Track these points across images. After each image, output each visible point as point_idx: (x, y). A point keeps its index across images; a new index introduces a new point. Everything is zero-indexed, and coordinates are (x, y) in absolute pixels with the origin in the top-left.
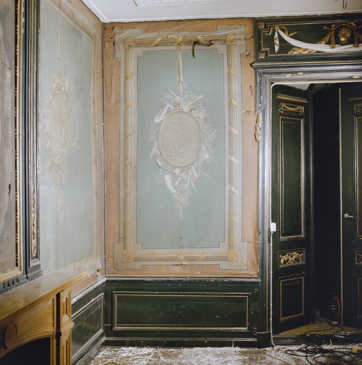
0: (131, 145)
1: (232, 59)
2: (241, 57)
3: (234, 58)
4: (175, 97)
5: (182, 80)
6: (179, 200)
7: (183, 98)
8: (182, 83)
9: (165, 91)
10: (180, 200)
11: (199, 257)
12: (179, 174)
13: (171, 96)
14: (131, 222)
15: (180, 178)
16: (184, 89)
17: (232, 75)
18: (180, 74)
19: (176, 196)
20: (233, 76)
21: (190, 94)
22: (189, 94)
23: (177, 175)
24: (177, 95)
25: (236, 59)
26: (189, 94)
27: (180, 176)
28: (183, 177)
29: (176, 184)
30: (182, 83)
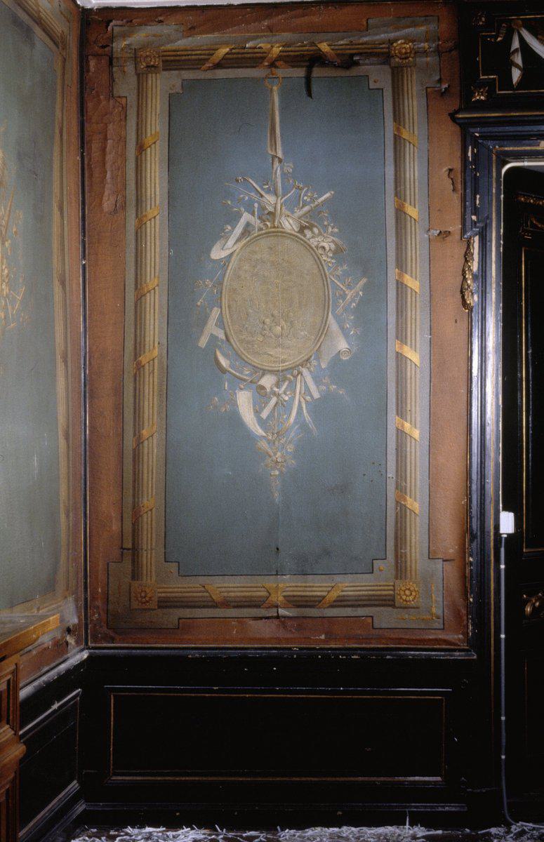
4: (262, 196)
6: (272, 454)
8: (280, 161)
9: (237, 181)
10: (275, 454)
12: (271, 389)
14: (151, 510)
15: (274, 400)
16: (284, 175)
17: (405, 143)
18: (275, 137)
20: (408, 144)
21: (302, 189)
24: (268, 191)
25: (415, 103)
26: (298, 188)
27: (275, 394)
28: (284, 396)
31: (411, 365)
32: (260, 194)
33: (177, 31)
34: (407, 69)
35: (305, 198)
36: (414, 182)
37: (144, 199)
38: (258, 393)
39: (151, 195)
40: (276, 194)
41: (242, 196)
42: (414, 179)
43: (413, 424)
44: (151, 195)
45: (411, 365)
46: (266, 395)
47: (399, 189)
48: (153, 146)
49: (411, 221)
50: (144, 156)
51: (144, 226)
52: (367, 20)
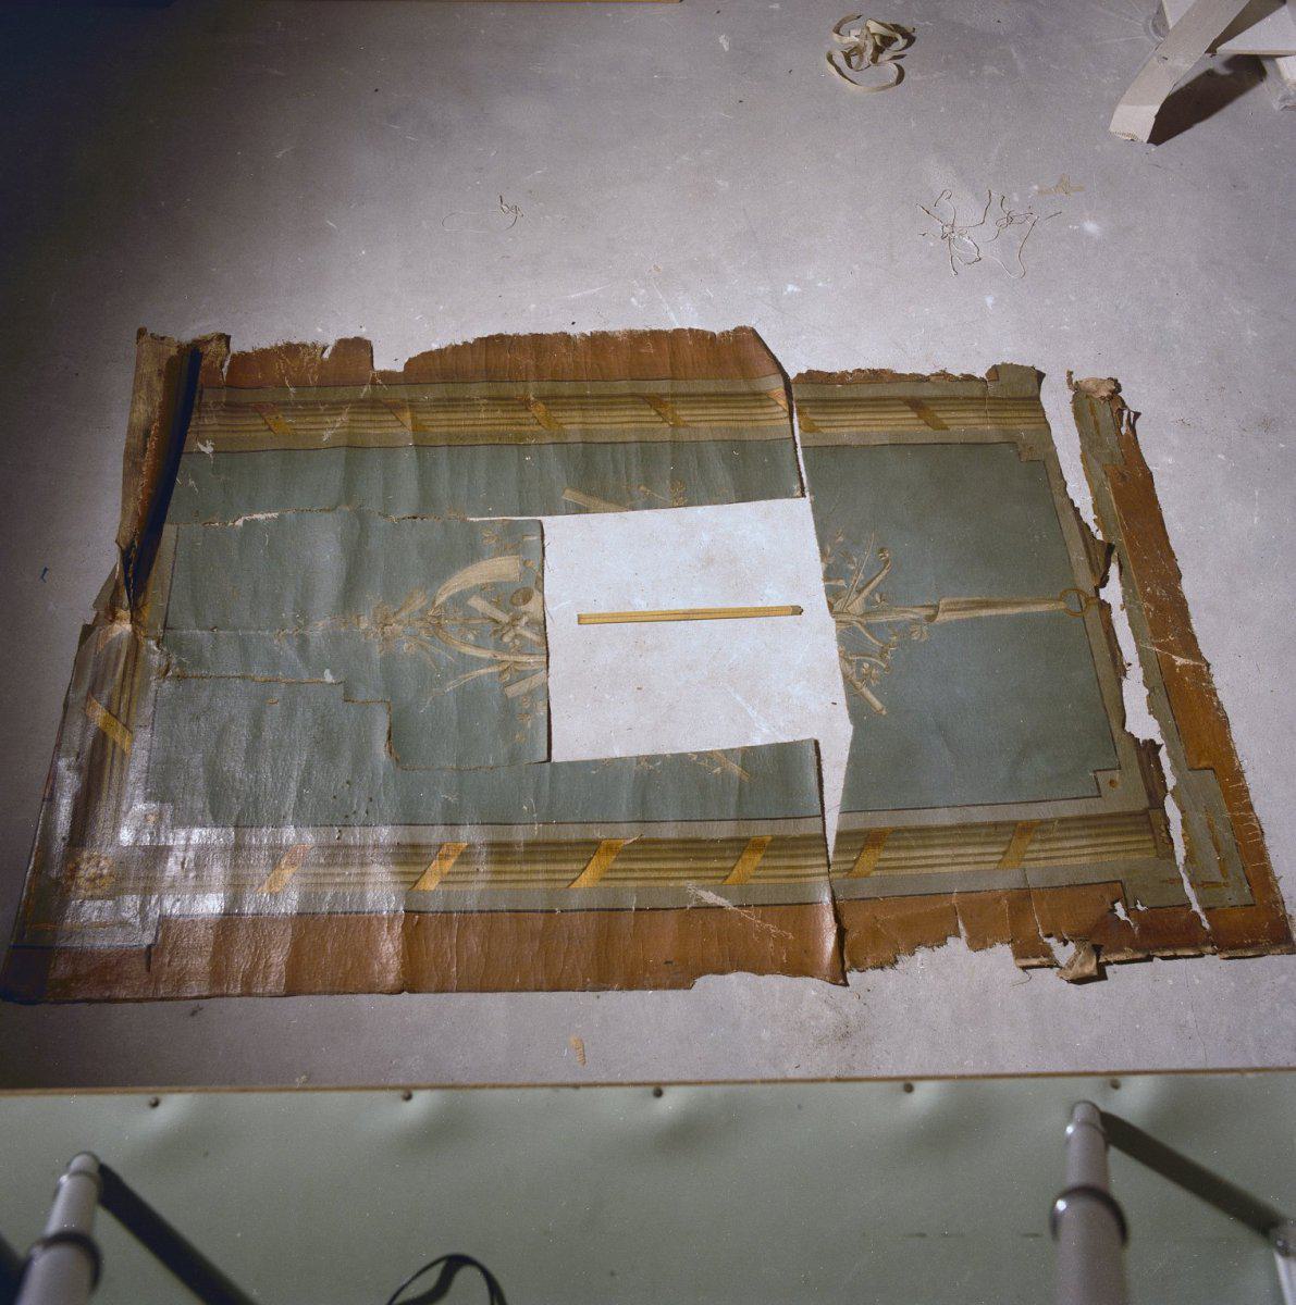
0: (625, 419)
1: (1084, 842)
2: (610, 910)
3: (1090, 850)
4: (859, 592)
5: (941, 617)
6: (398, 618)
7: (860, 622)
8: (931, 618)
9: (882, 550)
10: (399, 622)
11: (123, 719)
12: (525, 613)
13: (861, 576)
14: (270, 429)
15: (504, 618)
16: (905, 629)
17: (1003, 843)
18: (971, 609)
19: (419, 602)
20: (1002, 849)
21: (882, 657)
22: (883, 652)
23: (523, 608)
24: (868, 602)
25: (1084, 860)
26: (883, 652)
27: (515, 619)
28: (511, 634)
29: (477, 603)
30: (931, 618)
31: (572, 871)
32: (863, 589)
33: (1112, 455)
34: (823, 865)
35: (866, 665)
36: (927, 866)
37: (827, 410)
38: (518, 591)
39: (838, 420)
40: (867, 614)
41: (855, 559)
42: (935, 865)
43: (451, 878)
44: (838, 420)
45: (572, 871)
46: (514, 604)
47: (907, 835)
48: (921, 422)
49: (724, 869)
50: (904, 408)
51: (388, 411)
52: (1211, 769)
